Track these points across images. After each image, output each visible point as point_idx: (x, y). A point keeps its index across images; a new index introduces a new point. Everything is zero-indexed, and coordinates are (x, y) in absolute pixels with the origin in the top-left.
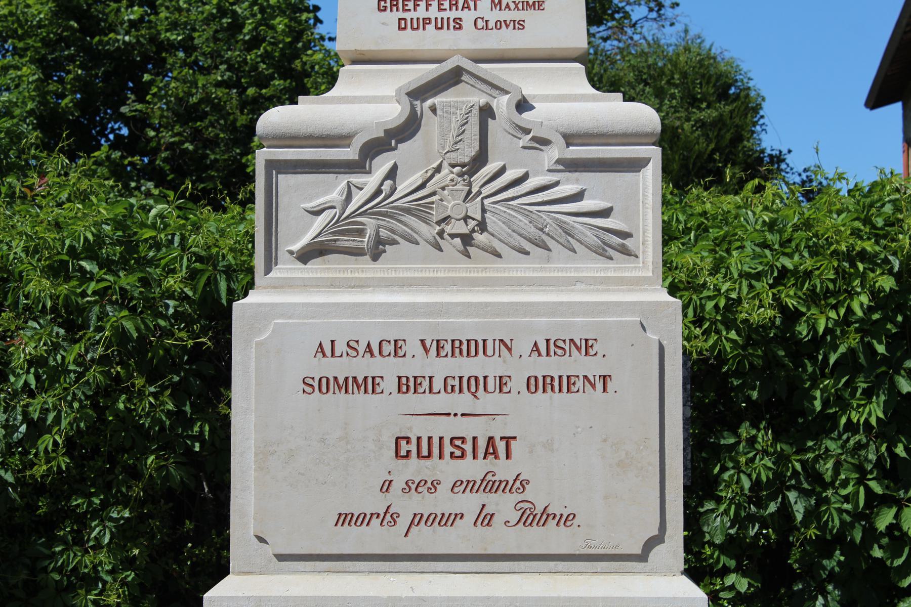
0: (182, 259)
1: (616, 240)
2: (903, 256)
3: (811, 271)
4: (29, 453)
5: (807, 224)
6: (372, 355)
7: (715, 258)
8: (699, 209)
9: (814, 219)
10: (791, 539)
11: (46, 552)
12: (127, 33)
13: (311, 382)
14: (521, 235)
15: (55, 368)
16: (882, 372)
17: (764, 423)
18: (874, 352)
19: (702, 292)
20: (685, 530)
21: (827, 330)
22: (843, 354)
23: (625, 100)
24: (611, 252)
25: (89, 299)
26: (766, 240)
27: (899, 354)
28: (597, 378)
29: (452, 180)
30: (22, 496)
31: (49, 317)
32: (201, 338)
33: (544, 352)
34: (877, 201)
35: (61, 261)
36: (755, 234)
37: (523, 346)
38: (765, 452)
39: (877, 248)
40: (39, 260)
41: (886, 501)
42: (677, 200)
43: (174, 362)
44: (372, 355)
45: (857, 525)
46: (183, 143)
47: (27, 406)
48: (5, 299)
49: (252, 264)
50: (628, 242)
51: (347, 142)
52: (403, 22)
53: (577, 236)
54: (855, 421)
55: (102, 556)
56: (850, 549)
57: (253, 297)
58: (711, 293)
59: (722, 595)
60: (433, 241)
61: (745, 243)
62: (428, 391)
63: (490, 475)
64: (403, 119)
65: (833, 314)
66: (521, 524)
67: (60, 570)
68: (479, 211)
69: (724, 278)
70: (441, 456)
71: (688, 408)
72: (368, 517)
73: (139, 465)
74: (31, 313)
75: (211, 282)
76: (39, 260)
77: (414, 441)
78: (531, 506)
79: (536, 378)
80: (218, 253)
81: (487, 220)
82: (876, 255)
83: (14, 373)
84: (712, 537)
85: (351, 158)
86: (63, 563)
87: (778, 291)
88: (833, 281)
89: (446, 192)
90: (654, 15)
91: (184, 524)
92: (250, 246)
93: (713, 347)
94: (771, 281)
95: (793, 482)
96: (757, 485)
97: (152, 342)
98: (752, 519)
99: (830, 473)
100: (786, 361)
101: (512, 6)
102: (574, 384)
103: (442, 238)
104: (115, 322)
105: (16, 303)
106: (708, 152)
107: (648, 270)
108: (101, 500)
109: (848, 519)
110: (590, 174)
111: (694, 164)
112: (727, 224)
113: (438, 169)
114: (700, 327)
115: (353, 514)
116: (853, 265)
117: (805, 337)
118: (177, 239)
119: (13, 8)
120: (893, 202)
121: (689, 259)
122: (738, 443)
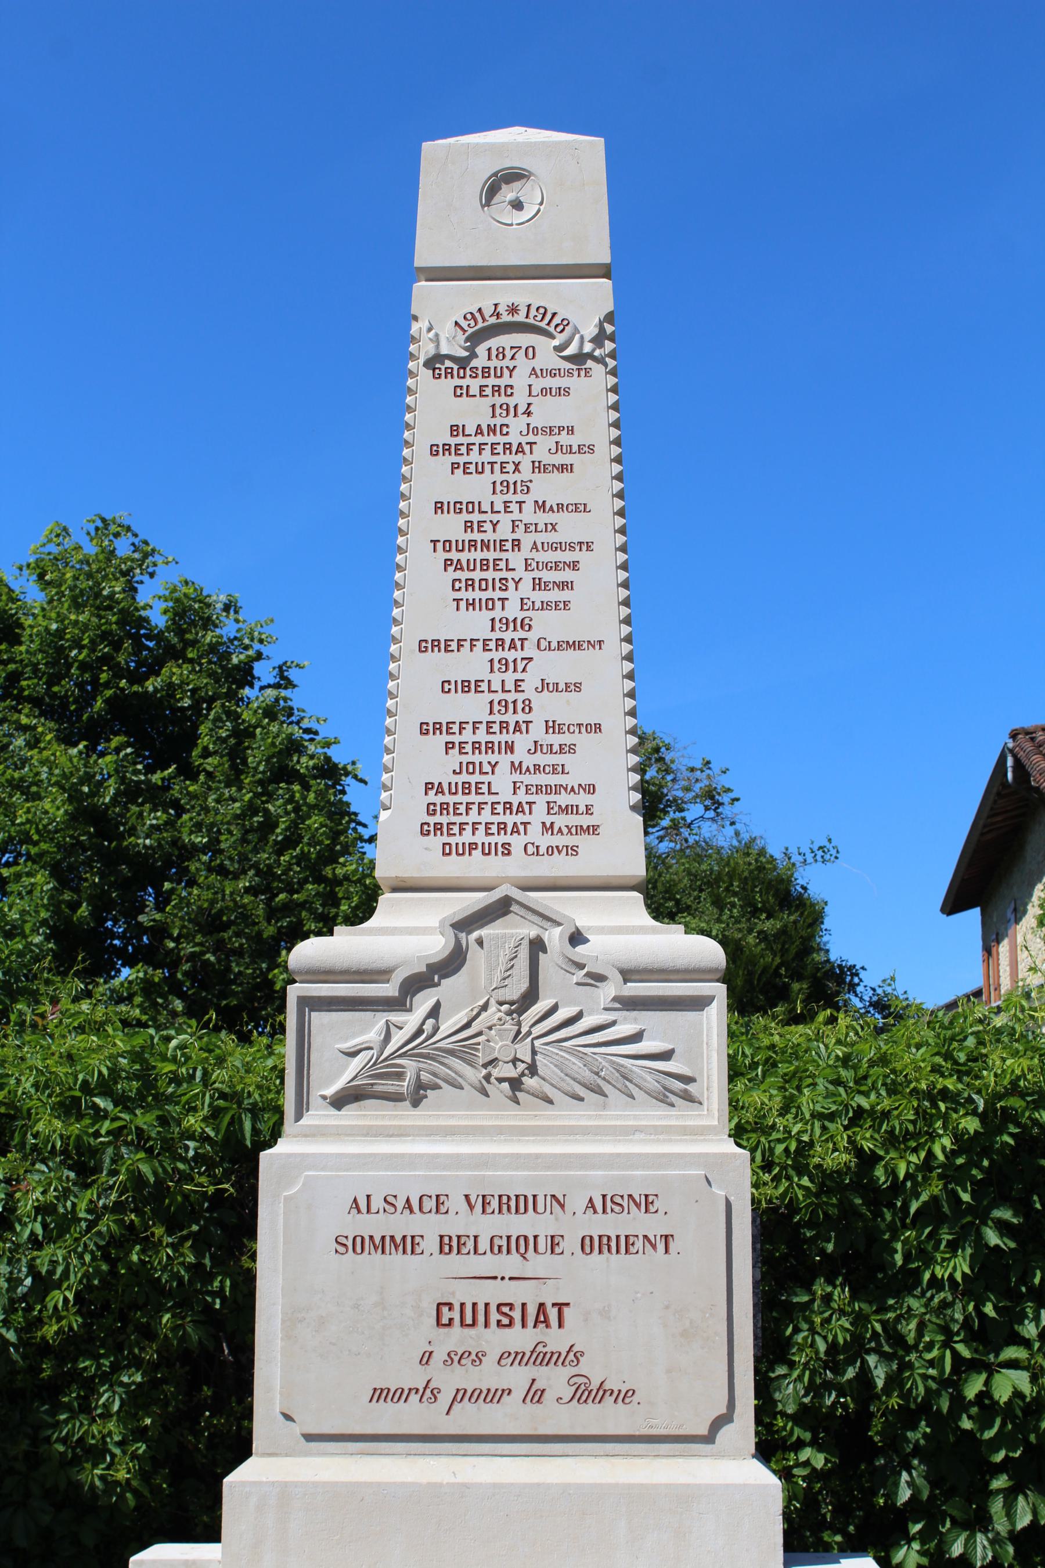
0: (204, 1095)
1: (678, 1085)
2: (988, 1094)
3: (889, 1112)
4: (34, 1309)
5: (883, 1060)
6: (412, 1211)
7: (784, 1097)
8: (766, 1042)
9: (891, 1054)
10: (872, 1408)
11: (49, 1420)
12: (147, 836)
13: (344, 1241)
14: (574, 1079)
15: (65, 1215)
16: (968, 1222)
17: (840, 1279)
18: (959, 1200)
19: (770, 1135)
20: (756, 1399)
21: (908, 1175)
22: (925, 1203)
23: (686, 933)
24: (673, 1098)
25: (102, 1139)
26: (839, 1076)
27: (985, 1203)
28: (658, 1238)
29: (500, 1019)
30: (24, 1357)
31: (58, 1159)
32: (223, 1183)
33: (599, 1208)
34: (959, 1034)
35: (73, 1097)
36: (828, 1070)
37: (577, 1203)
38: (842, 1312)
39: (960, 1086)
40: (50, 1096)
41: (975, 1366)
42: (743, 1030)
43: (193, 1209)
44: (412, 1211)
45: (943, 1393)
46: (203, 953)
47: (33, 1259)
48: (12, 1138)
49: (279, 1103)
50: (690, 1088)
51: (386, 977)
52: (447, 847)
53: (636, 1080)
54: (940, 1277)
55: (111, 1425)
56: (937, 1420)
57: (282, 1147)
58: (780, 1136)
59: (796, 1471)
60: (478, 1085)
61: (817, 1080)
62: (472, 1252)
63: (540, 1346)
64: (447, 953)
65: (913, 1158)
66: (575, 1400)
67: (64, 1441)
68: (529, 1053)
69: (794, 1118)
70: (487, 1325)
71: (758, 1270)
72: (406, 1392)
73: (153, 1324)
74: (39, 1154)
75: (236, 1121)
76: (50, 1096)
77: (457, 1307)
78: (586, 1381)
79: (591, 1237)
80: (243, 1090)
81: (538, 1063)
82: (959, 1093)
83: (20, 1221)
84: (784, 1406)
85: (390, 994)
86: (68, 1433)
87: (854, 1133)
88: (914, 1122)
89: (493, 1032)
90: (711, 814)
91: (201, 1390)
92: (278, 1082)
93: (783, 1195)
94: (846, 1123)
95: (873, 1344)
96: (833, 1348)
97: (169, 1187)
98: (828, 1386)
99: (913, 1335)
100: (864, 1210)
101: (565, 830)
102: (633, 1244)
103: (489, 1082)
104: (131, 1165)
105: (23, 1144)
106: (774, 967)
107: (713, 1117)
108: (110, 1362)
109: (934, 1386)
110: (649, 1013)
111: (759, 980)
112: (797, 1058)
113: (485, 1007)
114: (770, 1172)
115: (389, 1390)
116: (934, 1105)
117: (884, 1183)
118: (199, 1074)
119: (30, 816)
120: (976, 1034)
121: (757, 1097)
122: (813, 1301)
